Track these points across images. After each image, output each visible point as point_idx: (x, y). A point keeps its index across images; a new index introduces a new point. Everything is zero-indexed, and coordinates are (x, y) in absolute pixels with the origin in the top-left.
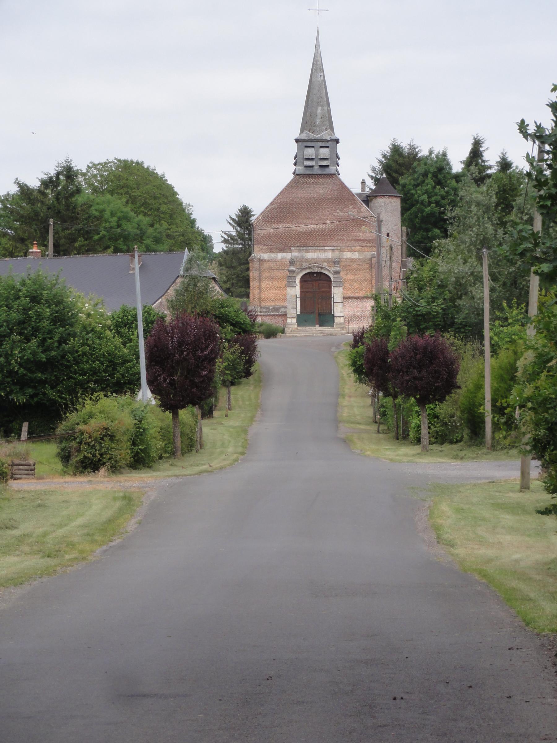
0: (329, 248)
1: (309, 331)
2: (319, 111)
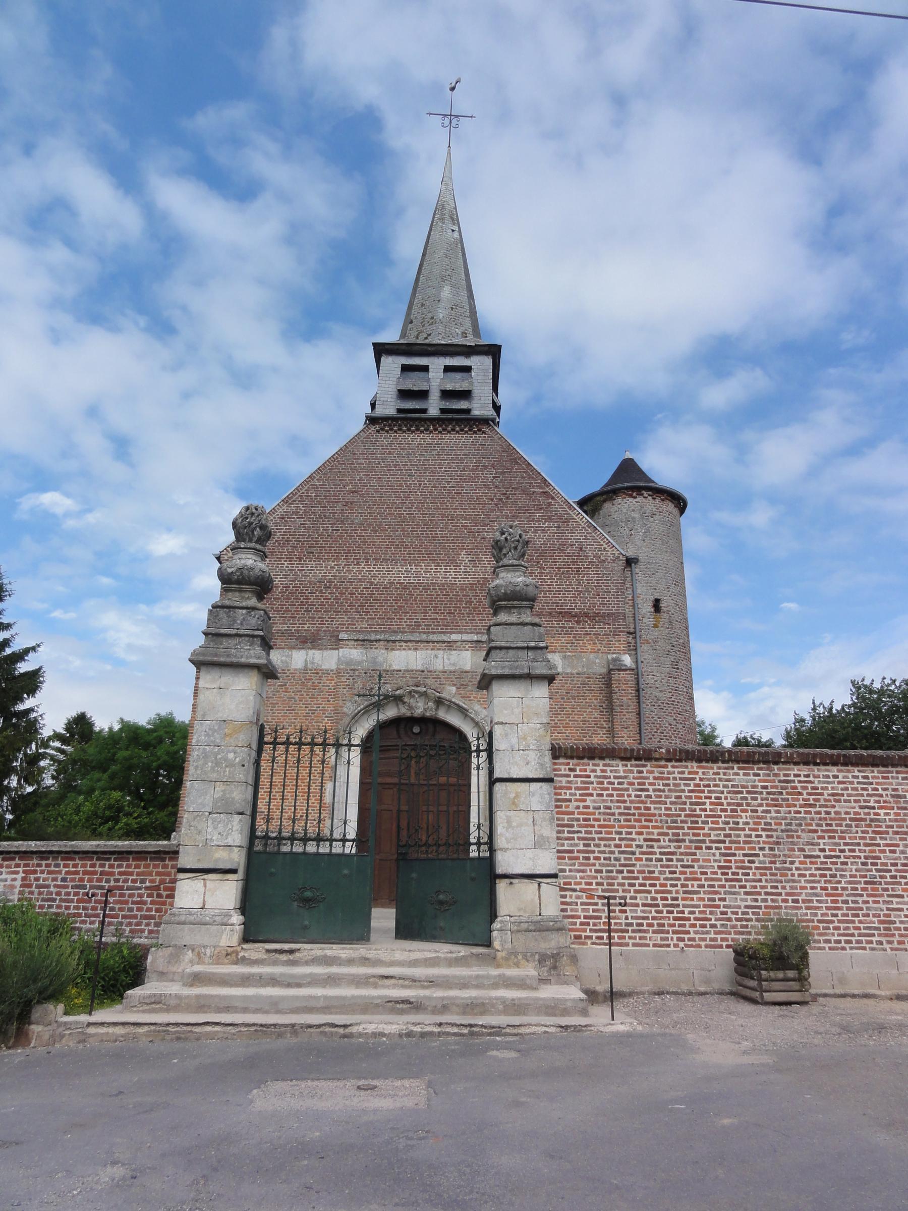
0: (466, 637)
1: (314, 981)
2: (446, 292)
